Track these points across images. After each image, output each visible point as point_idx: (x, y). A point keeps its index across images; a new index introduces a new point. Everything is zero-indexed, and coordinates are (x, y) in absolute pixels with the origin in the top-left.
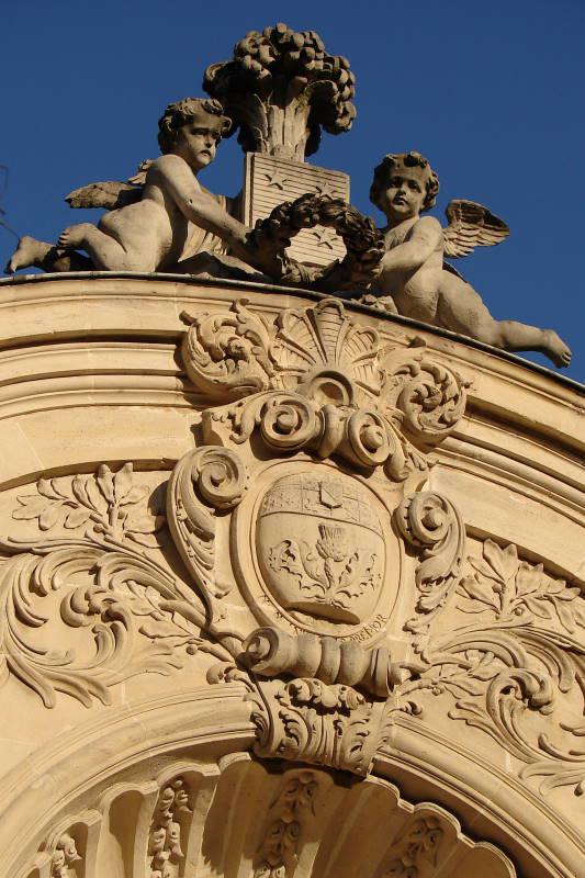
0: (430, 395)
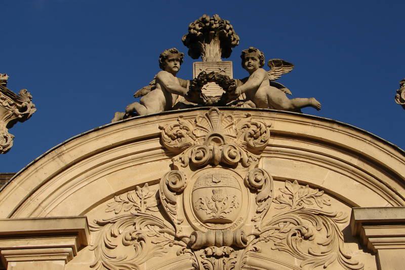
0: (255, 133)
